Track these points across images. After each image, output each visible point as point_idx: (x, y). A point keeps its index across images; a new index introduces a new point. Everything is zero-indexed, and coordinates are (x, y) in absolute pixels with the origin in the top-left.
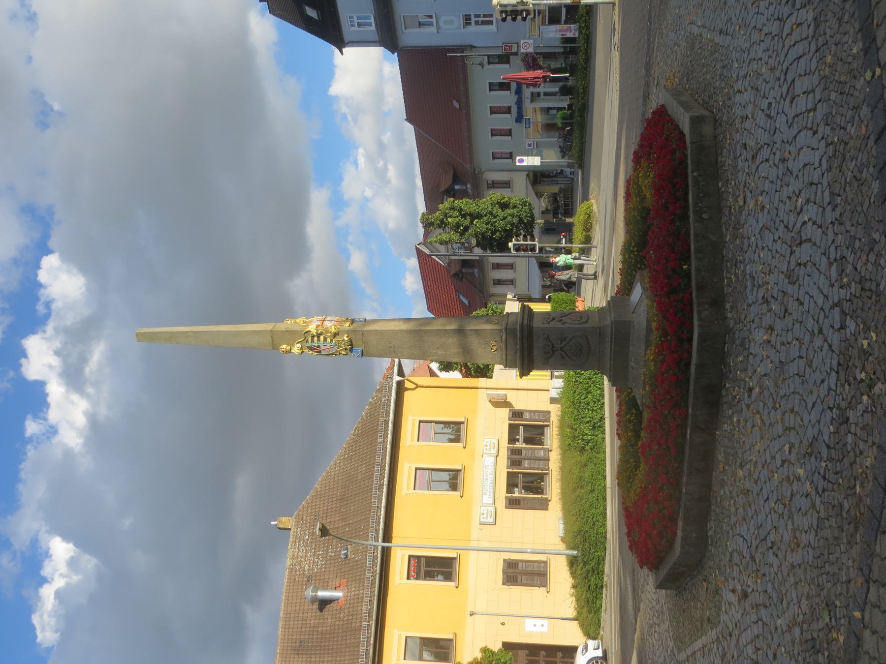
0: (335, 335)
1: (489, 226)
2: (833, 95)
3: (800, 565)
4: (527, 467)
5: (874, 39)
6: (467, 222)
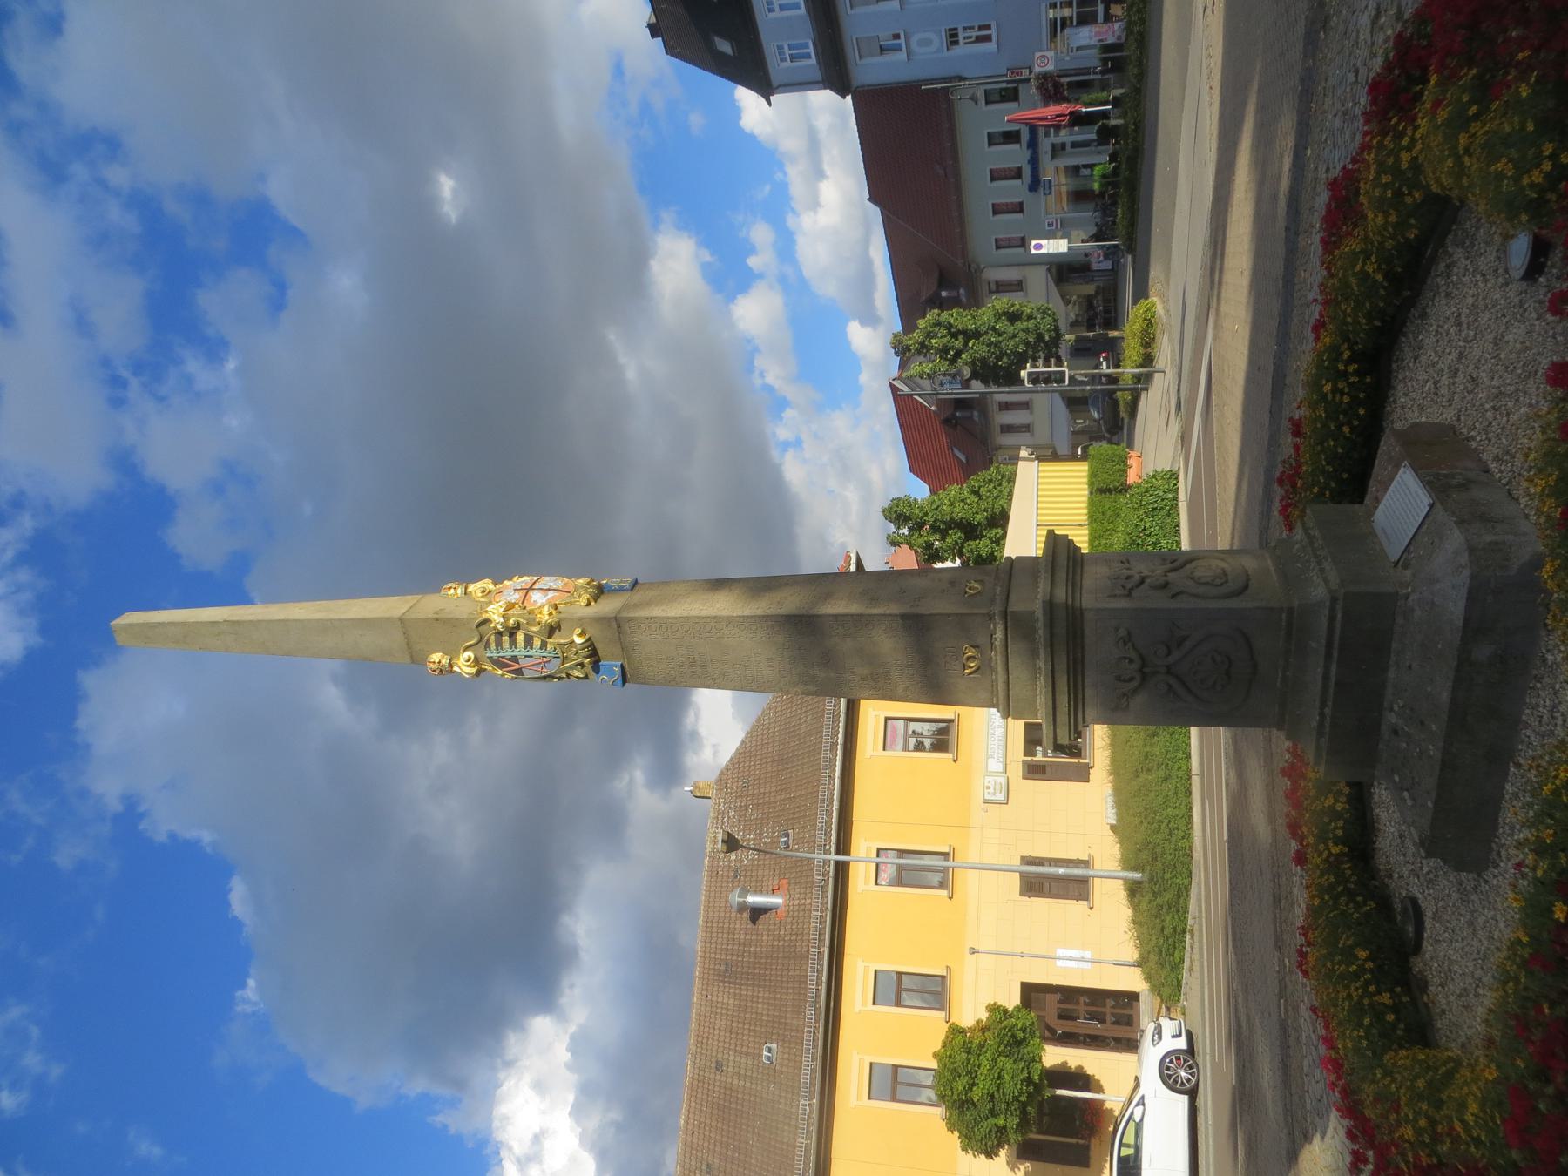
0: (552, 630)
6: (959, 344)
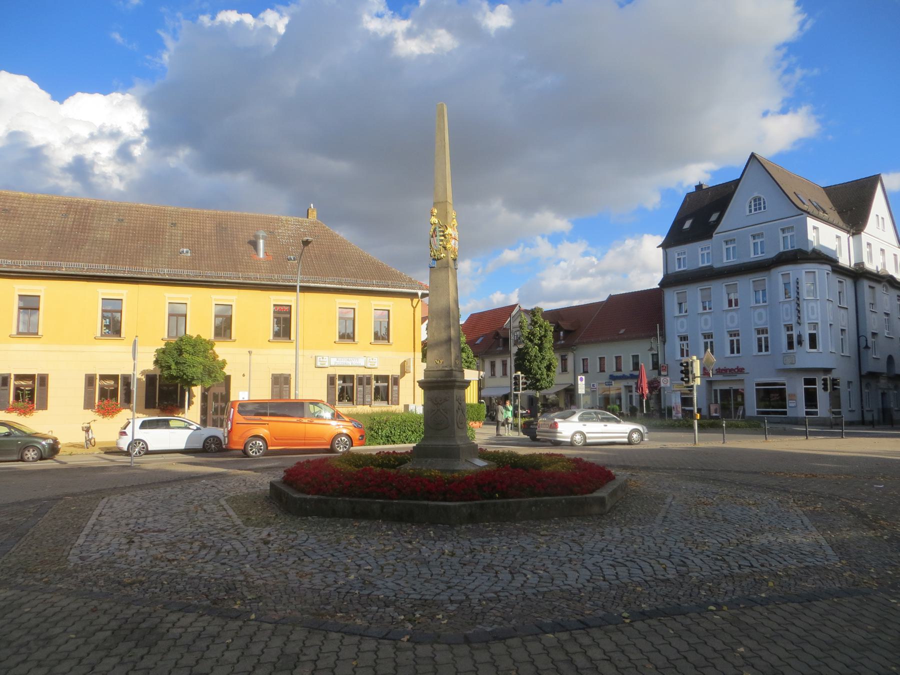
0: (445, 248)
2: (614, 592)
3: (287, 578)
4: (358, 389)
5: (650, 618)
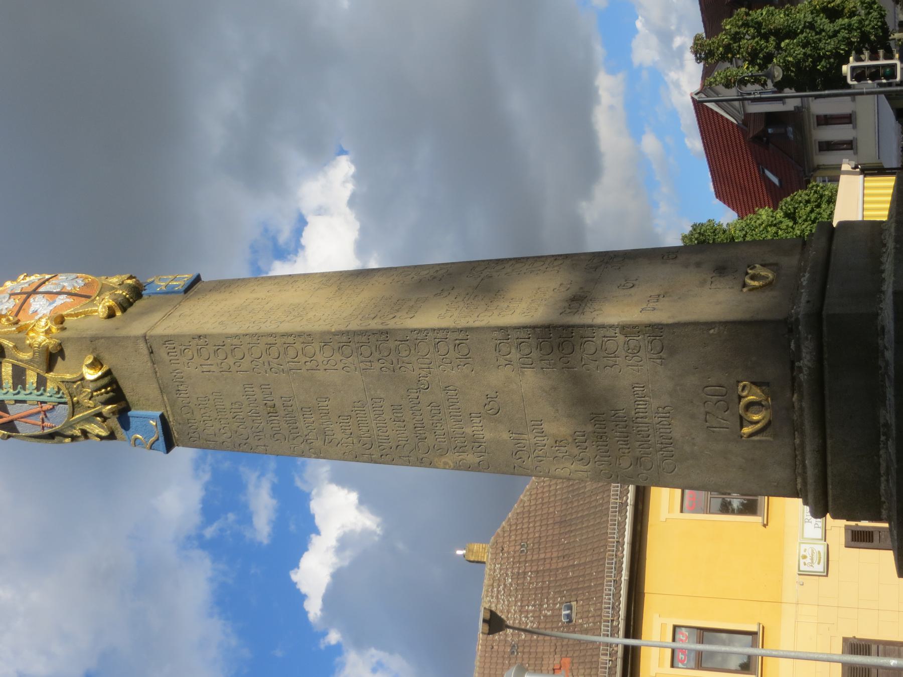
0: (52, 358)
1: (808, 51)
